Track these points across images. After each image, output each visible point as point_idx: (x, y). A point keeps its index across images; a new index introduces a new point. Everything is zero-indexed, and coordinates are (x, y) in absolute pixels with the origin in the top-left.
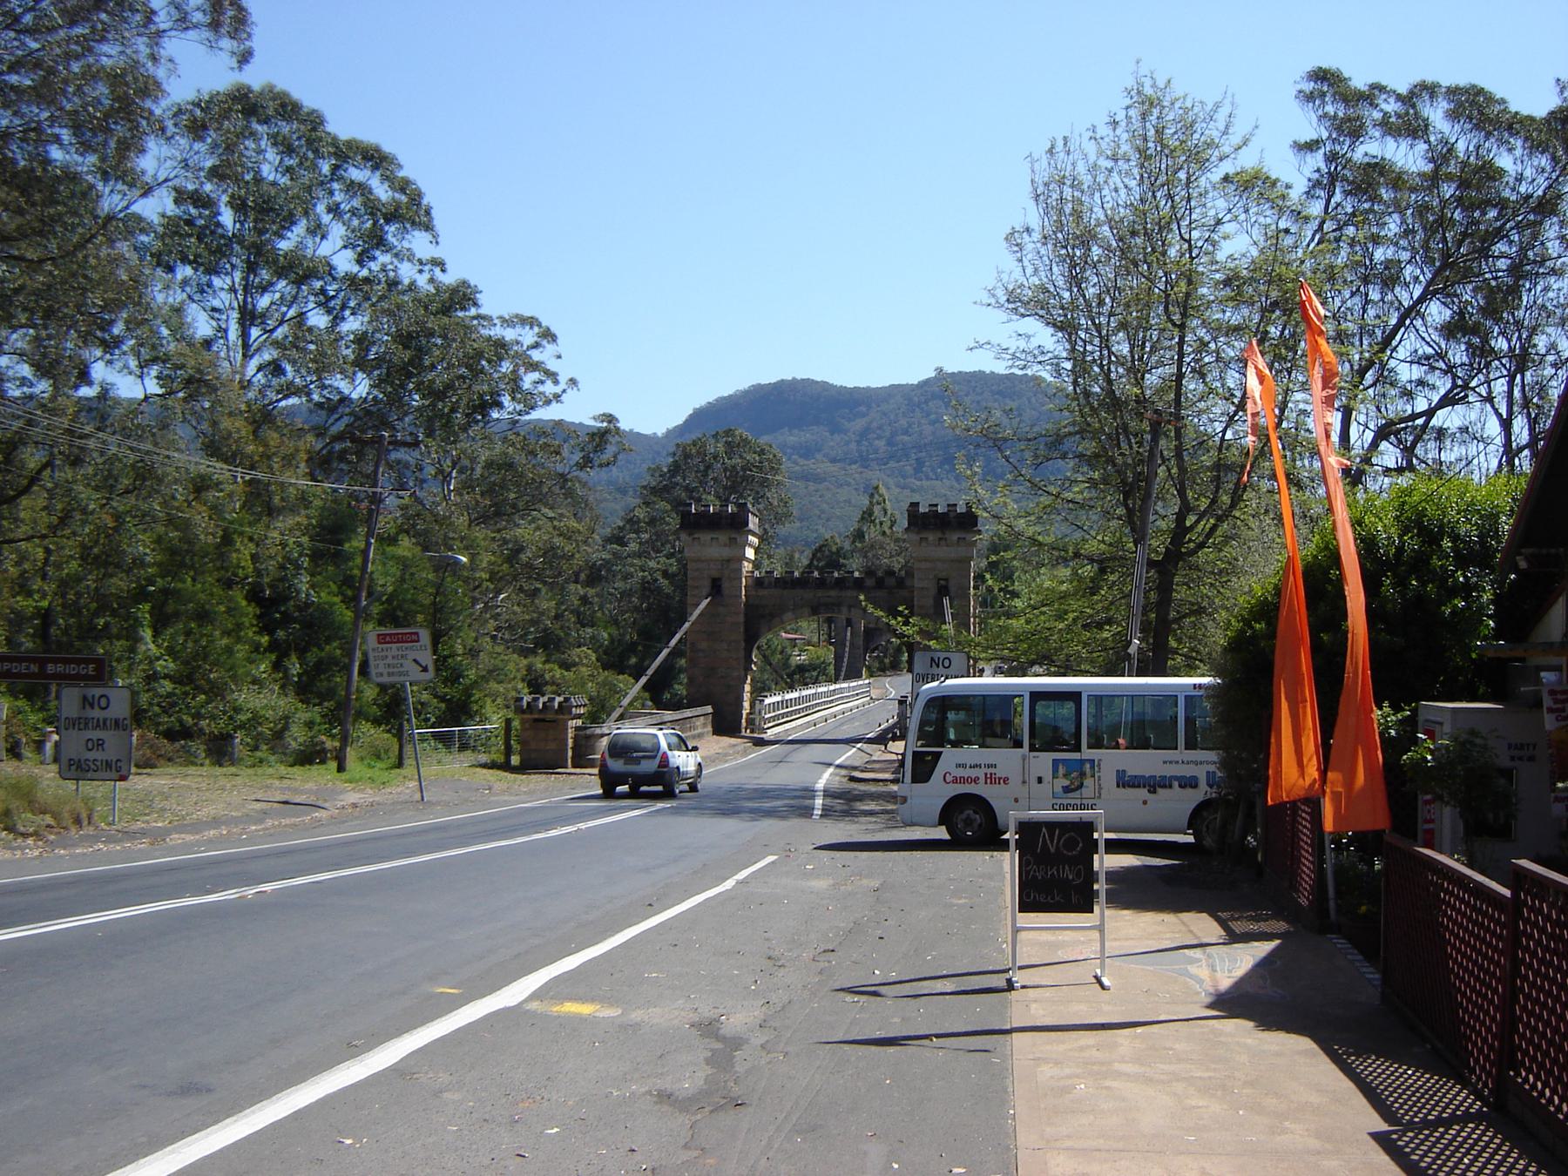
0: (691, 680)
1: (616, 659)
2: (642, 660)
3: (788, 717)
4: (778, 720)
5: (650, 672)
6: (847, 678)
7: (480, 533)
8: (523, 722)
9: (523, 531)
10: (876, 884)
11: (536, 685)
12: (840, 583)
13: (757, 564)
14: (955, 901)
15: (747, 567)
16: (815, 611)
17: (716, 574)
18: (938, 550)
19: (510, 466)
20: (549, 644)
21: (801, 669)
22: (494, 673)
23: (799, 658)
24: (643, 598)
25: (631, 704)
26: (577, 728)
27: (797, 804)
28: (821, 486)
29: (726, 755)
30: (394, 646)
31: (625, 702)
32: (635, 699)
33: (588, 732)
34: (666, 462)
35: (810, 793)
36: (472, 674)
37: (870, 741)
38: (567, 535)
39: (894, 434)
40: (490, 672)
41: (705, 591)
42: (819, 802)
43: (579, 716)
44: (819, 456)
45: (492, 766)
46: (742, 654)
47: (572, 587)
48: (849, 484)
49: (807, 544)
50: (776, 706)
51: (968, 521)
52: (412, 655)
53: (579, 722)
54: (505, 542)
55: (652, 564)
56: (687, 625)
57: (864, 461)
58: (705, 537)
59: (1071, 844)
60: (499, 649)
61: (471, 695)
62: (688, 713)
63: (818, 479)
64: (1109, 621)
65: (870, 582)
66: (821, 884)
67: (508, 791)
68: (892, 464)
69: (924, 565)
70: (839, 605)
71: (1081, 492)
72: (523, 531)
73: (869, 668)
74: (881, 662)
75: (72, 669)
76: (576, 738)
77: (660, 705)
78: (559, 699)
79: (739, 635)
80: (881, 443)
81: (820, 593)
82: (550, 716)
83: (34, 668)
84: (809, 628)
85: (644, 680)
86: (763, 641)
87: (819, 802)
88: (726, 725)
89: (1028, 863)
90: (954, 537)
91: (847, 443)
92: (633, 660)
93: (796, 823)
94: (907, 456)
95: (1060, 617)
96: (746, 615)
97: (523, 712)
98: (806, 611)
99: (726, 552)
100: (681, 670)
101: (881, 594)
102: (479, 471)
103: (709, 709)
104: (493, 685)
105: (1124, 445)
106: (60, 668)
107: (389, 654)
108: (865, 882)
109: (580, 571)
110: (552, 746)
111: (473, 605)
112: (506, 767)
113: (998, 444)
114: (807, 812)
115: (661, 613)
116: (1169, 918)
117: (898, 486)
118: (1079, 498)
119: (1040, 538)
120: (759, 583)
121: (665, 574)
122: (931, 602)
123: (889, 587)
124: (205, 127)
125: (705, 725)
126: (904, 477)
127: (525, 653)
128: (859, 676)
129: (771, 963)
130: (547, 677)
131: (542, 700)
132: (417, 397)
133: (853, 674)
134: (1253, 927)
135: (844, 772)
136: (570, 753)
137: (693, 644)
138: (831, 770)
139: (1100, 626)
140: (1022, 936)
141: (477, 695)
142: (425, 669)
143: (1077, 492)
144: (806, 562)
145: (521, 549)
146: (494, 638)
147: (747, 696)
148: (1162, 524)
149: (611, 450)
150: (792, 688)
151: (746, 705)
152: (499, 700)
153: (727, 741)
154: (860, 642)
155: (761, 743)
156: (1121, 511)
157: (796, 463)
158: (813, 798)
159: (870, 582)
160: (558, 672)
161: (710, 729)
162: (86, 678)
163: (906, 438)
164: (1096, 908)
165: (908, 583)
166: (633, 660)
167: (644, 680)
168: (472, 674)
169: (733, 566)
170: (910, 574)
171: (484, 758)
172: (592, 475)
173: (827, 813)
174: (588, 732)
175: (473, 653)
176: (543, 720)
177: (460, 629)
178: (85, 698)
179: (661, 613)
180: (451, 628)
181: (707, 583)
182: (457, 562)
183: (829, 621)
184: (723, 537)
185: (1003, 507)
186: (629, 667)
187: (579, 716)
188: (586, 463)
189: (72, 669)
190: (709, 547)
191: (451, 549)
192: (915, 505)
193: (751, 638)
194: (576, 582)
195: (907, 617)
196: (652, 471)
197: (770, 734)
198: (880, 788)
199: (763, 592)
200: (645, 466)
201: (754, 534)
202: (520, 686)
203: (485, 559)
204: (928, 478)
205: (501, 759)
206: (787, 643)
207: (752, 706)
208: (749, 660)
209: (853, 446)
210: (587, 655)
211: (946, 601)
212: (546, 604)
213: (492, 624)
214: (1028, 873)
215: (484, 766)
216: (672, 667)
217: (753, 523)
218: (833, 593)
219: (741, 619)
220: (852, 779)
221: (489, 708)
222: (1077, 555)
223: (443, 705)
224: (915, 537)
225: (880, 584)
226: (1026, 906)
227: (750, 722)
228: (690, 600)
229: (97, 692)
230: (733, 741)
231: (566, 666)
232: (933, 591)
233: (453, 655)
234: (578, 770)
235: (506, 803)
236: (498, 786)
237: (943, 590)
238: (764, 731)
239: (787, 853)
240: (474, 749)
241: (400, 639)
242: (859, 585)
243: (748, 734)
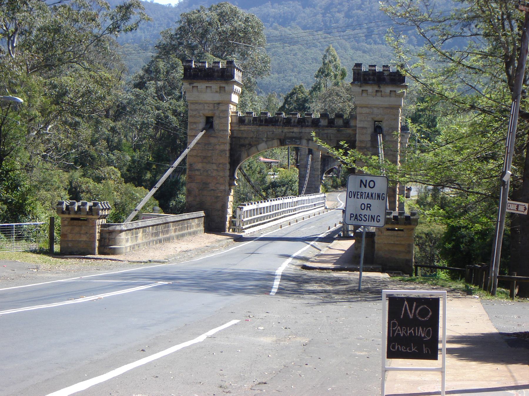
0: (189, 192)
1: (135, 176)
2: (155, 176)
3: (261, 221)
4: (254, 223)
5: (158, 185)
6: (308, 192)
7: (35, 79)
8: (63, 220)
9: (66, 79)
10: (305, 340)
11: (75, 193)
12: (301, 122)
13: (242, 105)
14: (358, 353)
15: (232, 108)
16: (282, 143)
17: (209, 114)
18: (374, 99)
19: (57, 30)
20: (84, 161)
21: (274, 185)
22: (44, 183)
23: (272, 177)
24: (156, 128)
25: (144, 208)
26: (103, 226)
27: (261, 284)
28: (295, 47)
29: (213, 247)
31: (139, 207)
32: (148, 205)
33: (111, 228)
34: (174, 28)
35: (271, 276)
36: (27, 184)
37: (321, 240)
38: (101, 82)
39: (350, 9)
40: (41, 182)
41: (201, 126)
42: (276, 283)
43: (104, 217)
44: (293, 24)
45: (40, 252)
46: (227, 173)
47: (105, 121)
48: (316, 46)
49: (283, 90)
50: (252, 212)
51: (397, 79)
53: (104, 221)
54: (54, 87)
55: (165, 104)
56: (187, 151)
57: (328, 30)
58: (202, 85)
59: (423, 313)
60: (48, 165)
61: (25, 200)
62: (186, 216)
63: (293, 42)
64: (494, 157)
65: (324, 122)
66: (267, 340)
67: (50, 270)
68: (349, 32)
69: (365, 110)
70: (300, 139)
71: (477, 61)
72: (66, 79)
73: (325, 186)
74: (334, 181)
76: (101, 233)
77: (166, 209)
78: (90, 204)
79: (225, 159)
80: (341, 16)
81: (286, 130)
82: (83, 216)
84: (281, 154)
85: (154, 191)
86: (245, 163)
87: (276, 283)
88: (214, 225)
89: (394, 325)
90: (387, 89)
91: (315, 15)
92: (148, 176)
93: (261, 298)
94: (360, 25)
95: (459, 151)
96: (231, 144)
97: (63, 212)
98: (276, 142)
99: (217, 98)
100: (183, 184)
101: (331, 131)
102: (34, 33)
103: (202, 213)
104: (43, 192)
105: (507, 27)
108: (298, 339)
109: (110, 108)
110: (84, 238)
111: (29, 132)
112: (50, 252)
113: (417, 23)
114: (266, 290)
115: (169, 143)
116: (501, 367)
117: (353, 48)
118: (476, 64)
119: (446, 94)
120: (241, 121)
121: (175, 113)
122: (369, 138)
123: (338, 126)
125: (198, 225)
126: (358, 42)
127: (67, 168)
128: (316, 191)
129: (221, 390)
130: (84, 187)
131: (77, 204)
133: (312, 189)
135: (299, 262)
136: (97, 244)
137: (191, 165)
138: (290, 260)
139: (486, 159)
140: (390, 375)
141: (30, 199)
143: (472, 60)
144: (281, 104)
145: (65, 93)
146: (44, 157)
147: (230, 205)
149: (134, 18)
150: (265, 199)
151: (230, 211)
152: (47, 204)
153: (214, 237)
154: (318, 165)
155: (239, 239)
156: (504, 76)
157: (276, 29)
158: (273, 280)
159: (324, 122)
160: (92, 184)
161: (202, 228)
163: (360, 12)
164: (440, 356)
165: (352, 123)
166: (148, 176)
167: (154, 191)
168: (27, 184)
169: (222, 108)
170: (353, 117)
171: (34, 246)
172: (121, 36)
173: (281, 291)
174: (111, 228)
175: (28, 168)
176: (78, 219)
177: (18, 151)
179: (169, 143)
180: (12, 149)
181: (203, 120)
182: (18, 102)
183: (297, 150)
184: (215, 86)
185: (423, 69)
186: (146, 181)
187: (104, 217)
188: (115, 28)
190: (205, 93)
191: (14, 92)
192: (358, 65)
193: (234, 162)
194: (107, 116)
195: (346, 150)
196: (164, 33)
197: (246, 233)
198: (325, 274)
199: (243, 128)
200: (162, 29)
201: (238, 84)
202: (63, 193)
203: (39, 100)
204: (375, 43)
205: (46, 247)
206: (265, 166)
207: (234, 212)
208: (232, 177)
209: (319, 17)
210: (113, 173)
211: (380, 138)
212: (86, 131)
213: (42, 147)
214: (394, 331)
215: (34, 252)
216: (177, 182)
217: (238, 76)
218: (296, 130)
219: (228, 147)
220: (304, 267)
221: (39, 209)
222: (473, 107)
223: (5, 207)
224: (357, 89)
225: (331, 123)
226: (392, 354)
227: (233, 223)
228: (189, 132)
230: (219, 237)
231: (98, 180)
232: (370, 130)
233: (13, 170)
234: (103, 257)
235: (49, 279)
236: (43, 266)
237: (378, 129)
238: (242, 230)
239: (247, 318)
240: (27, 239)
242: (315, 123)
243: (231, 232)
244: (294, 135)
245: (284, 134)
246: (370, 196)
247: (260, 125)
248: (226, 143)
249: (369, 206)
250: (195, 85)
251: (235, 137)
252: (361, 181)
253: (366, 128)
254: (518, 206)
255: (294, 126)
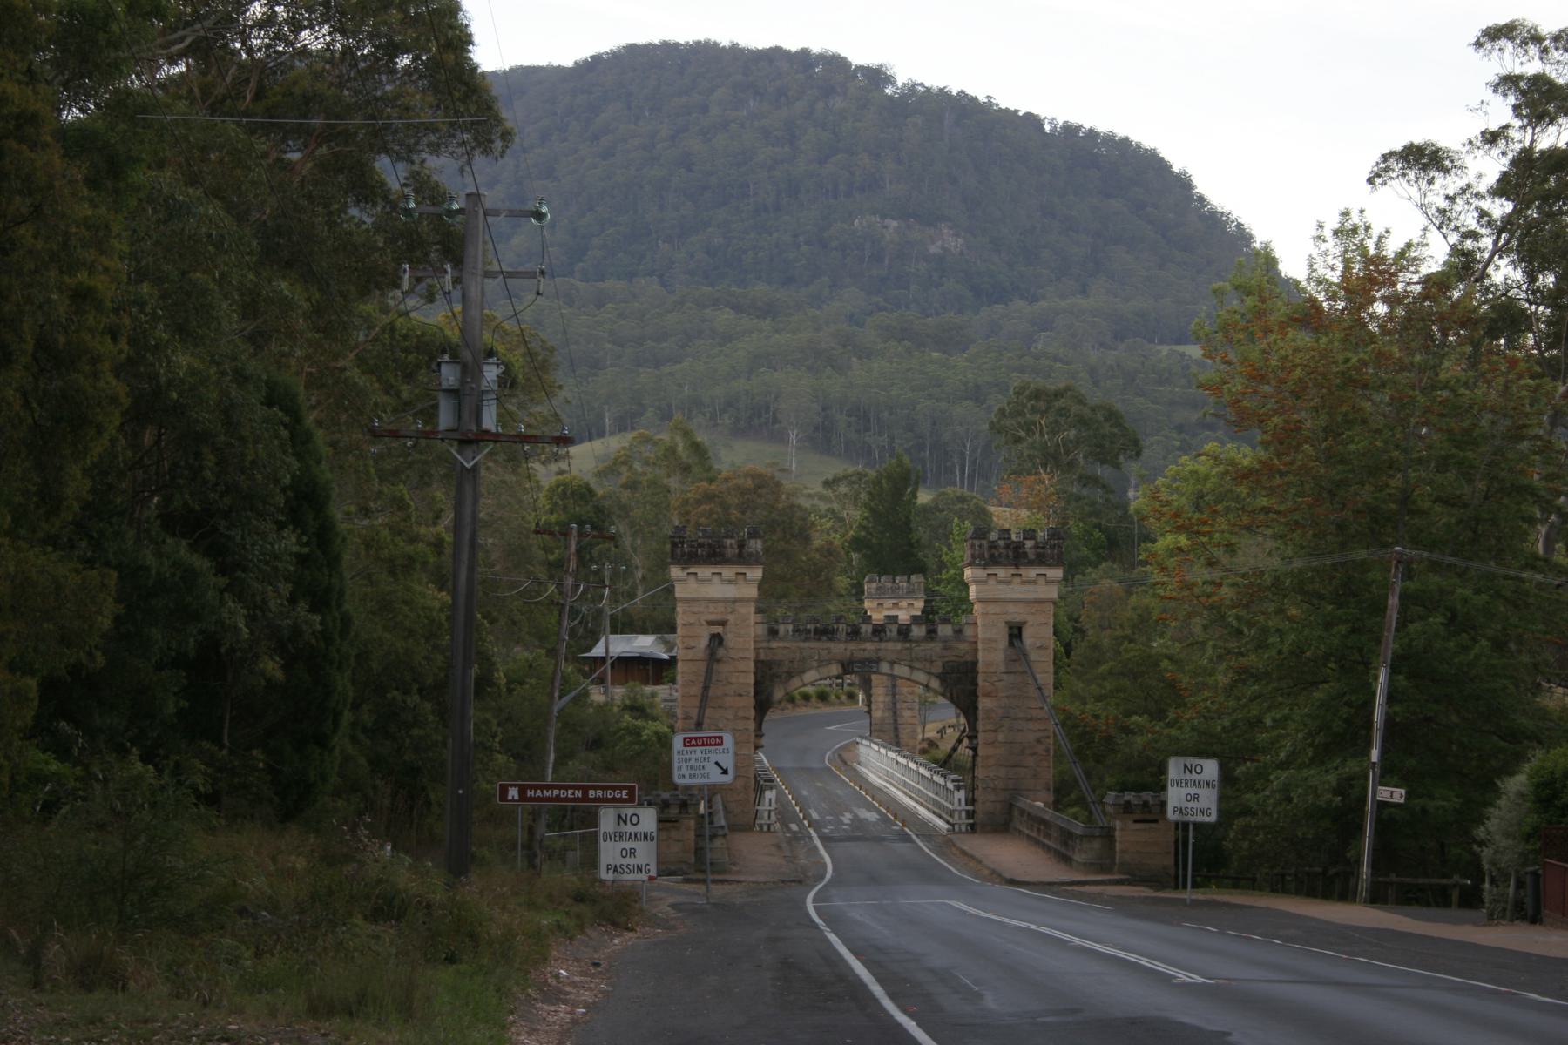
46: (752, 726)
52: (714, 758)
75: (609, 794)
83: (579, 794)
106: (599, 793)
107: (693, 756)
124: (438, 145)
132: (1332, 665)
142: (725, 772)
162: (621, 800)
229: (630, 811)
241: (704, 742)
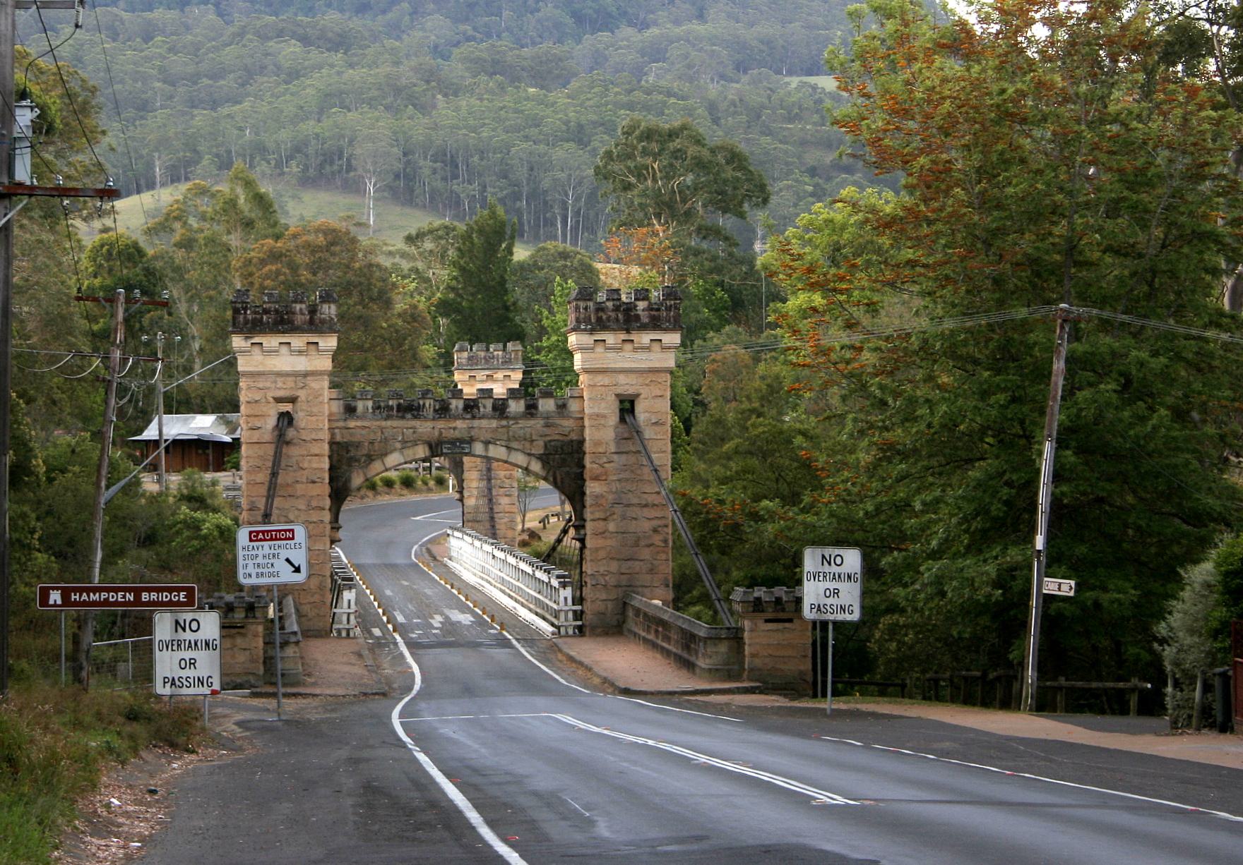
30: (266, 544)
52: (284, 554)
75: (165, 596)
106: (154, 596)
107: (260, 552)
134: (903, 806)
142: (297, 570)
148: (976, 218)
162: (179, 604)
178: (177, 622)
189: (165, 596)
218: (459, 424)
229: (188, 616)
244: (457, 434)
245: (437, 433)
246: (837, 577)
247: (388, 418)
248: (323, 455)
249: (836, 592)
250: (256, 340)
251: (338, 443)
252: (823, 557)
253: (604, 416)
254: (1060, 584)
255: (456, 418)
